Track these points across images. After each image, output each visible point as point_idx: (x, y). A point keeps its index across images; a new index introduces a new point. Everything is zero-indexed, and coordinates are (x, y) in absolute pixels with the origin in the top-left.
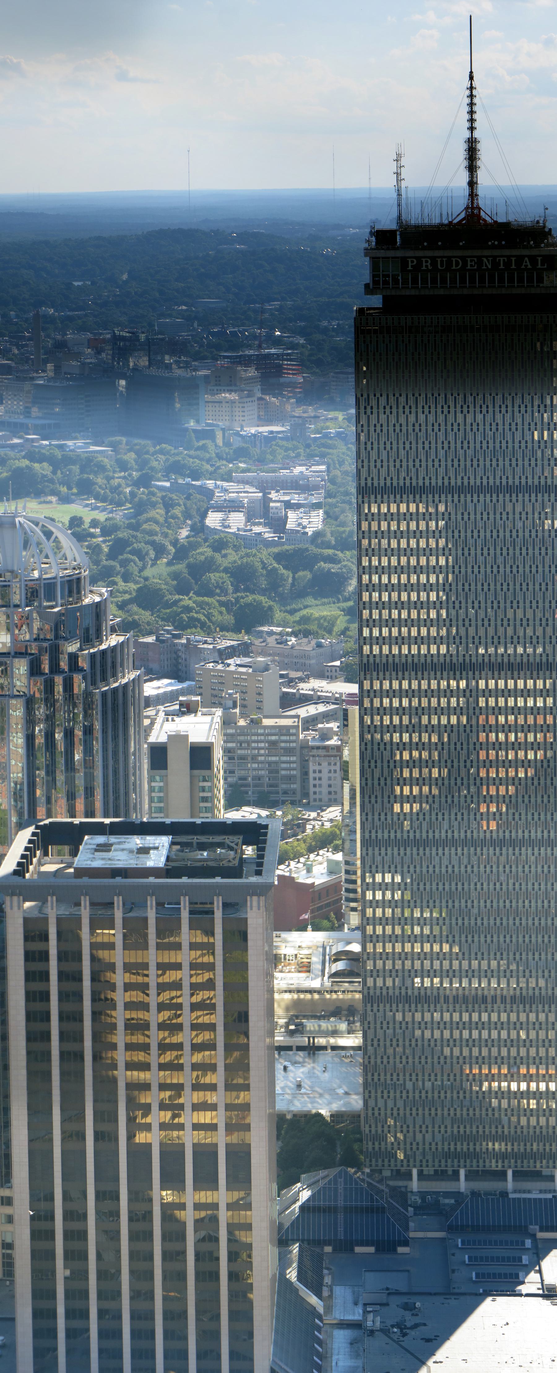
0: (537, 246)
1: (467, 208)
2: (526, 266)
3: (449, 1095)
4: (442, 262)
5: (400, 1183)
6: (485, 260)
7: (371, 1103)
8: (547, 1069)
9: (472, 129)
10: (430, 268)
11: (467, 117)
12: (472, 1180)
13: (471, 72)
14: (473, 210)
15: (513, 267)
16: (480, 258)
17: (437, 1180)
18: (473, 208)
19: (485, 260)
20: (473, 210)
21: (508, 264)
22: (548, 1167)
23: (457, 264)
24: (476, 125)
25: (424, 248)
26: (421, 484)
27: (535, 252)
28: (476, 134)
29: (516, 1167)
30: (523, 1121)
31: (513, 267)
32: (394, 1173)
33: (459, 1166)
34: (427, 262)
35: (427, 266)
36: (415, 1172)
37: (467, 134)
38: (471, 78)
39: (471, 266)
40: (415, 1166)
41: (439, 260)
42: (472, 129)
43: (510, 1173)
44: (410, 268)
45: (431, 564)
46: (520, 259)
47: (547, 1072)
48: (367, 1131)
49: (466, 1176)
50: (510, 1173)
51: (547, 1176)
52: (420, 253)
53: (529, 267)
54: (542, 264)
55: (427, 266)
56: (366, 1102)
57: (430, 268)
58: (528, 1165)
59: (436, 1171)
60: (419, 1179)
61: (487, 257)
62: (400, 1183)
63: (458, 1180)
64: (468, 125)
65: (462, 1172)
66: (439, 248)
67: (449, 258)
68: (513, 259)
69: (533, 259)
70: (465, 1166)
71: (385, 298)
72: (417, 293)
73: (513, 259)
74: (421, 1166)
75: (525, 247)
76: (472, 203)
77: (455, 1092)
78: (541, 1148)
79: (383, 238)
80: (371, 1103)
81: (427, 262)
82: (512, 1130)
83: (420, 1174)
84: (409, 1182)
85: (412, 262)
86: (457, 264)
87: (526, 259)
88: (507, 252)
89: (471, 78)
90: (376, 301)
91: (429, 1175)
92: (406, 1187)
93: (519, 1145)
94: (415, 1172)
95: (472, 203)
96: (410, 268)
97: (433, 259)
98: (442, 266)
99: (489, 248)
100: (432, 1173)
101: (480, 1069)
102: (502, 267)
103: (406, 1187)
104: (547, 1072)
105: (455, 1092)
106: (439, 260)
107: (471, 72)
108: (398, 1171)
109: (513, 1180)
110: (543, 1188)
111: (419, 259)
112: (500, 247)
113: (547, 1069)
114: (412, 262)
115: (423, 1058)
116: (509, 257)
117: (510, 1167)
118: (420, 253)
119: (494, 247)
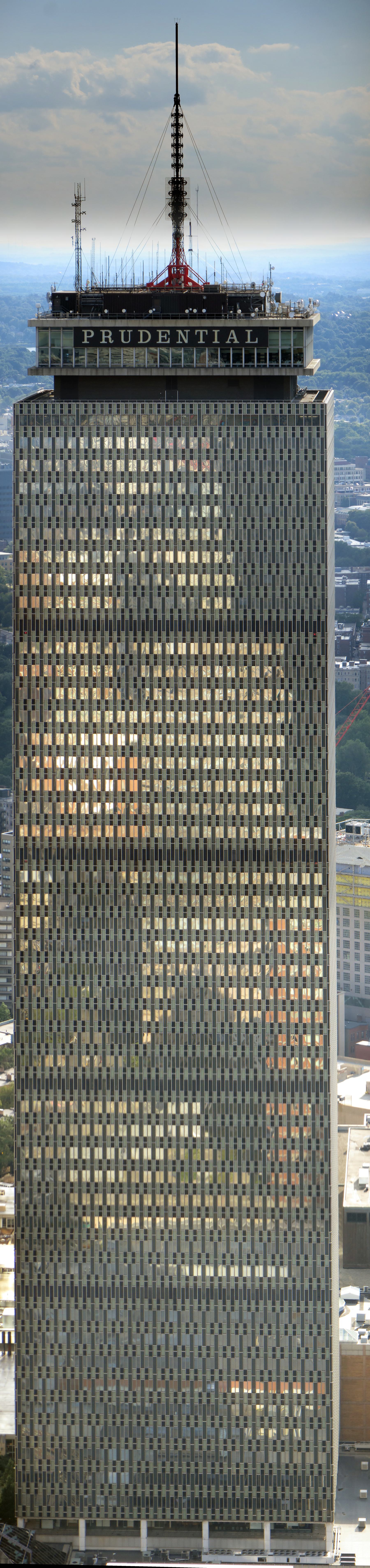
0: (247, 315)
1: (170, 268)
2: (232, 340)
3: (126, 1421)
4: (126, 334)
5: (63, 1539)
6: (180, 332)
7: (25, 1429)
8: (254, 1388)
9: (177, 166)
10: (111, 341)
11: (172, 151)
12: (157, 1535)
13: (177, 95)
14: (178, 270)
15: (216, 342)
16: (173, 330)
17: (112, 1535)
18: (178, 265)
19: (180, 332)
20: (178, 270)
21: (209, 338)
22: (255, 1519)
23: (145, 337)
24: (183, 161)
25: (104, 317)
26: (192, 617)
27: (243, 323)
28: (183, 173)
29: (213, 1518)
30: (273, 1458)
31: (216, 342)
32: (58, 1525)
33: (139, 1516)
34: (107, 334)
35: (107, 340)
36: (82, 1524)
37: (172, 173)
38: (177, 102)
39: (163, 339)
40: (82, 1516)
41: (122, 332)
42: (177, 166)
43: (205, 1526)
44: (86, 342)
45: (107, 720)
46: (225, 331)
47: (254, 1391)
48: (20, 1469)
49: (272, 1531)
50: (205, 1526)
51: (256, 1530)
52: (97, 323)
53: (236, 342)
54: (253, 339)
55: (107, 340)
56: (18, 1428)
57: (111, 341)
58: (229, 1516)
59: (113, 1523)
60: (88, 1534)
61: (182, 329)
62: (63, 1539)
63: (138, 1535)
64: (172, 161)
65: (144, 1525)
66: (122, 317)
67: (135, 330)
68: (216, 332)
69: (240, 331)
70: (147, 1517)
71: (57, 379)
72: (94, 374)
73: (216, 332)
74: (90, 1516)
75: (234, 316)
76: (178, 260)
77: (135, 1416)
78: (271, 1493)
79: (63, 303)
80: (25, 1429)
81: (107, 334)
82: (258, 1470)
83: (90, 1526)
84: (75, 1538)
85: (89, 334)
86: (145, 337)
87: (233, 332)
88: (207, 323)
89: (177, 102)
90: (45, 384)
91: (102, 1528)
92: (71, 1544)
93: (217, 1488)
94: (82, 1524)
95: (178, 260)
96: (86, 342)
97: (115, 331)
98: (126, 339)
99: (185, 317)
100: (108, 1525)
101: (241, 1387)
102: (201, 342)
103: (71, 1544)
104: (254, 1391)
105: (135, 1416)
106: (122, 332)
107: (177, 95)
108: (63, 1523)
109: (210, 1536)
110: (248, 1547)
111: (97, 330)
112: (201, 316)
113: (254, 1388)
114: (89, 334)
115: (93, 1369)
116: (210, 329)
117: (205, 1518)
118: (97, 323)
119: (192, 316)
